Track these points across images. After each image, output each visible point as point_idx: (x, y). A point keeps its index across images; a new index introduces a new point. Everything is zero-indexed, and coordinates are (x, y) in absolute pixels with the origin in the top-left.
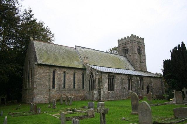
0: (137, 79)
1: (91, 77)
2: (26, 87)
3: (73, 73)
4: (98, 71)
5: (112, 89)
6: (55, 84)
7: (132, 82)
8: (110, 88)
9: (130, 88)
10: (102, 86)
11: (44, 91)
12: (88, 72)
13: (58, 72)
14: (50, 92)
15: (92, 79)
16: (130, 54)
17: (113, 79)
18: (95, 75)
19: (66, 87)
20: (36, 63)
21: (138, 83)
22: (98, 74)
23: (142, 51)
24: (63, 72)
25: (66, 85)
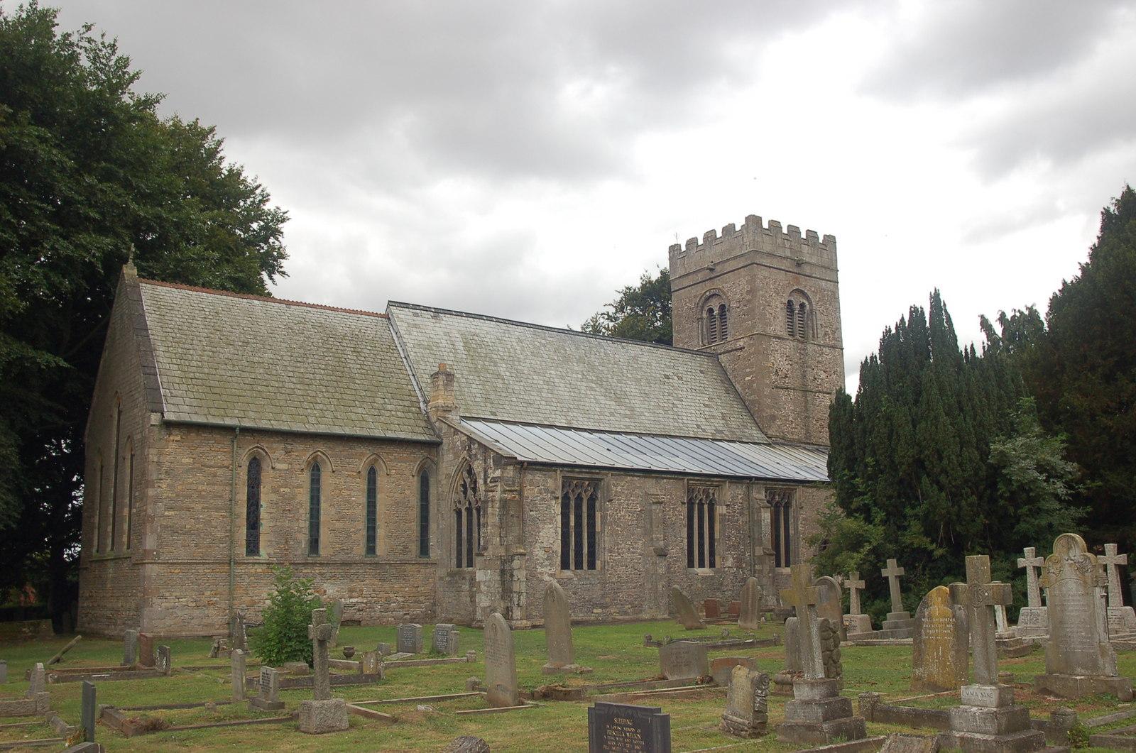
0: (748, 496)
1: (465, 492)
2: (101, 548)
3: (362, 465)
4: (505, 461)
5: (585, 559)
6: (262, 529)
7: (717, 518)
8: (572, 554)
10: (521, 541)
11: (201, 569)
12: (448, 464)
14: (230, 575)
15: (473, 500)
16: (737, 337)
17: (592, 500)
18: (485, 482)
19: (321, 545)
20: (155, 418)
22: (498, 473)
23: (821, 319)
24: (309, 463)
25: (325, 536)
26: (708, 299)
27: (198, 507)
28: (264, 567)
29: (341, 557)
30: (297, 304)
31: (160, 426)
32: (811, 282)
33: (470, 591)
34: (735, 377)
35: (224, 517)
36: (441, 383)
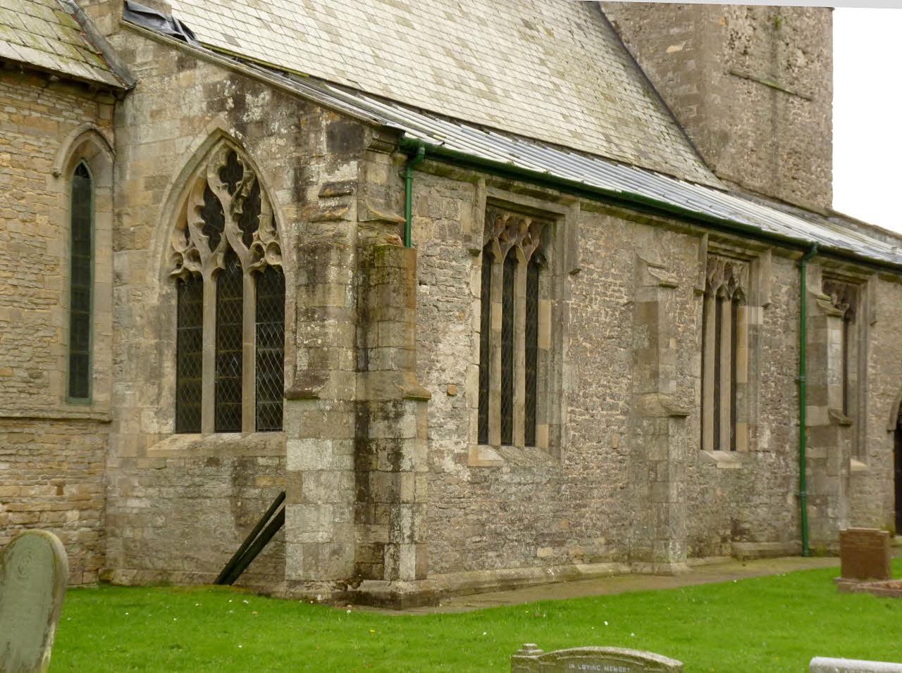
1: (213, 227)
5: (519, 416)
15: (240, 248)
17: (536, 265)
18: (299, 195)
34: (641, 47)
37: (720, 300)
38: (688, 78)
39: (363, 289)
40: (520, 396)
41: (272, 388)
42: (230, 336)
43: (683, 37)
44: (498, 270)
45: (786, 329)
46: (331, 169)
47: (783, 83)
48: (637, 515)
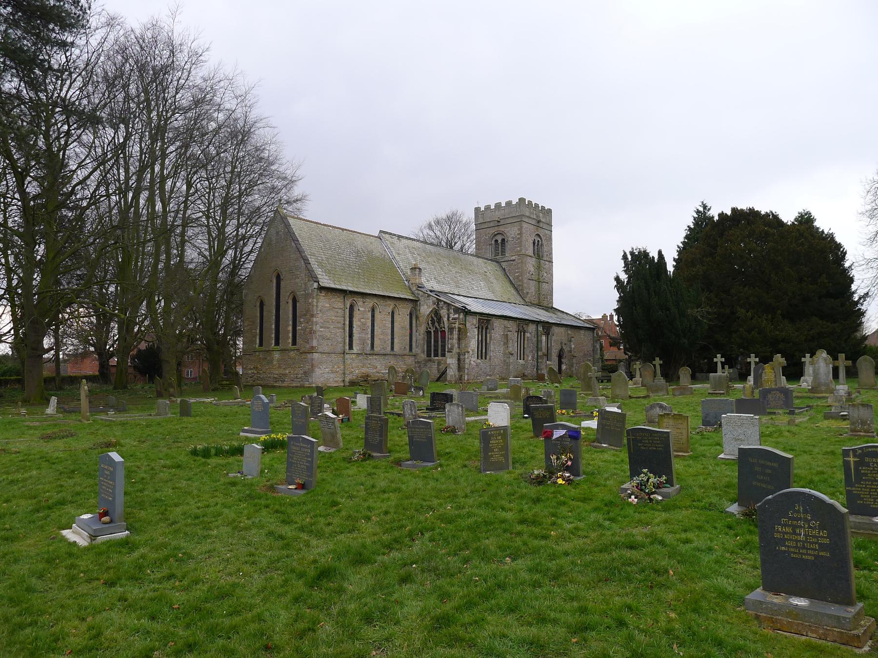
1: (433, 323)
5: (484, 354)
9: (522, 355)
13: (362, 308)
14: (344, 358)
15: (438, 327)
17: (487, 329)
18: (448, 320)
21: (539, 341)
22: (456, 316)
23: (545, 248)
25: (377, 342)
26: (495, 235)
27: (332, 327)
28: (356, 355)
29: (383, 352)
30: (346, 230)
31: (317, 289)
32: (542, 230)
33: (438, 368)
35: (341, 332)
36: (417, 272)
37: (521, 332)
38: (520, 281)
39: (459, 335)
40: (484, 351)
41: (443, 350)
42: (436, 341)
43: (518, 272)
44: (480, 330)
45: (534, 337)
46: (454, 315)
47: (541, 280)
48: (505, 372)
